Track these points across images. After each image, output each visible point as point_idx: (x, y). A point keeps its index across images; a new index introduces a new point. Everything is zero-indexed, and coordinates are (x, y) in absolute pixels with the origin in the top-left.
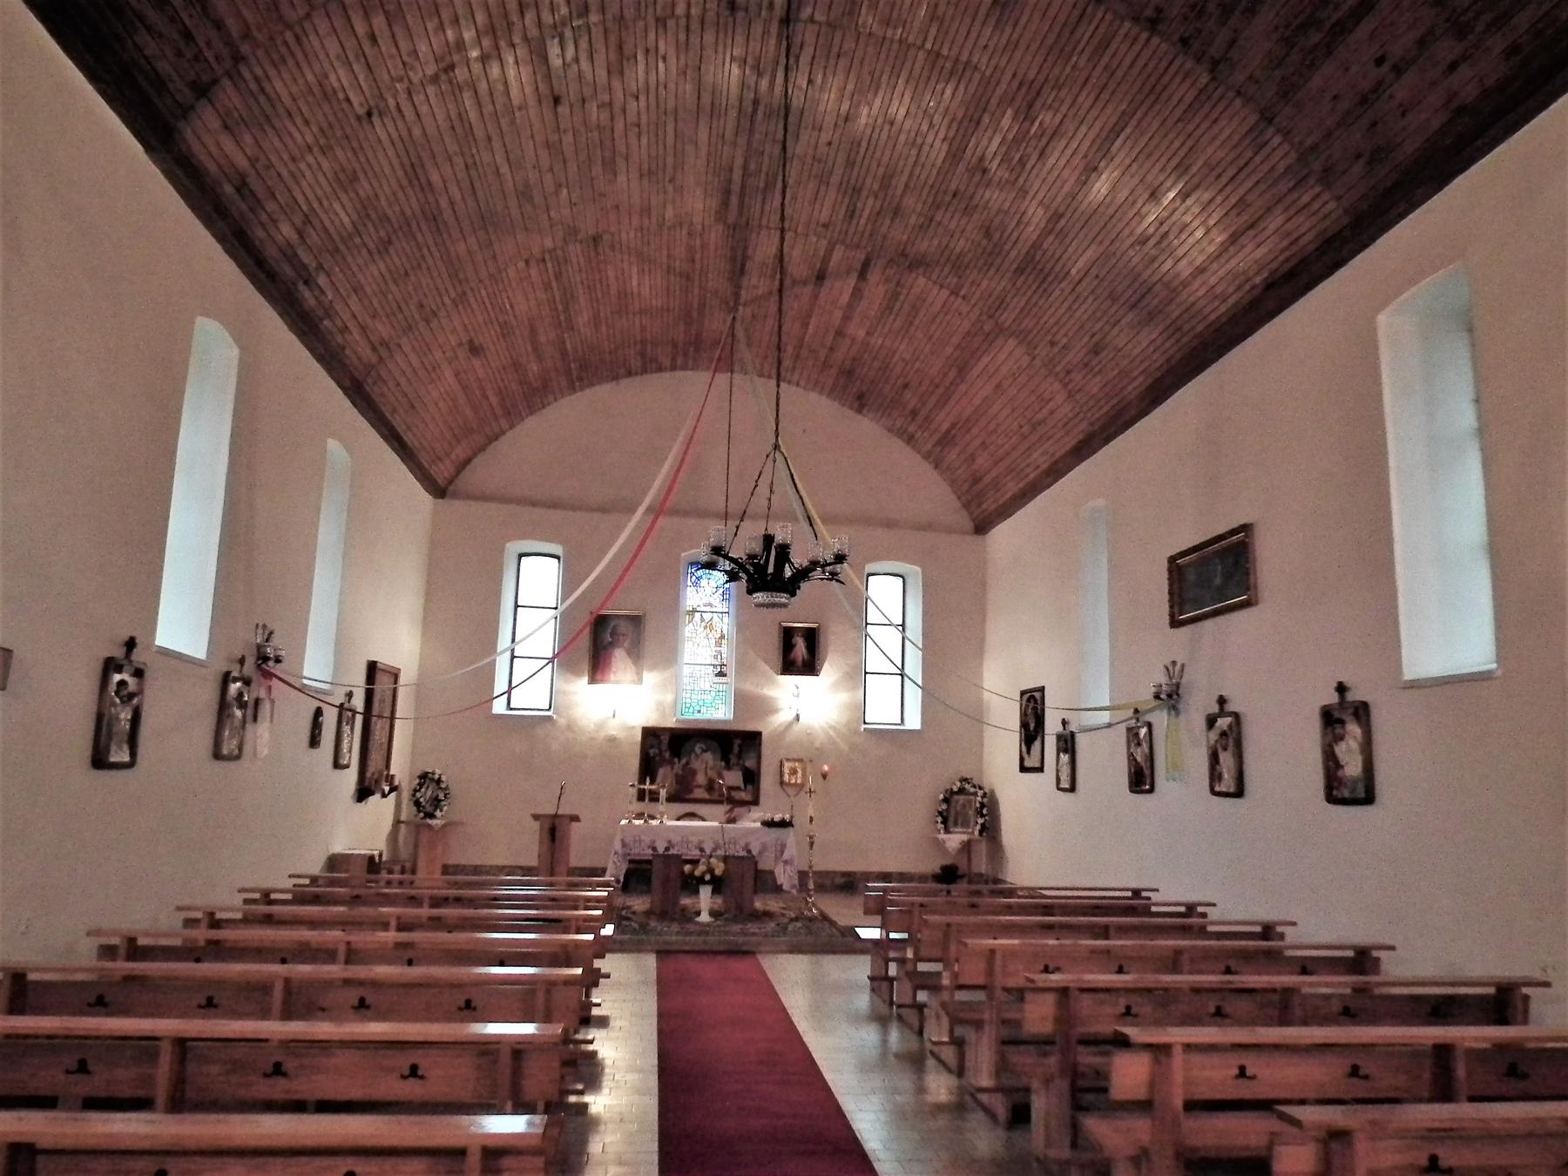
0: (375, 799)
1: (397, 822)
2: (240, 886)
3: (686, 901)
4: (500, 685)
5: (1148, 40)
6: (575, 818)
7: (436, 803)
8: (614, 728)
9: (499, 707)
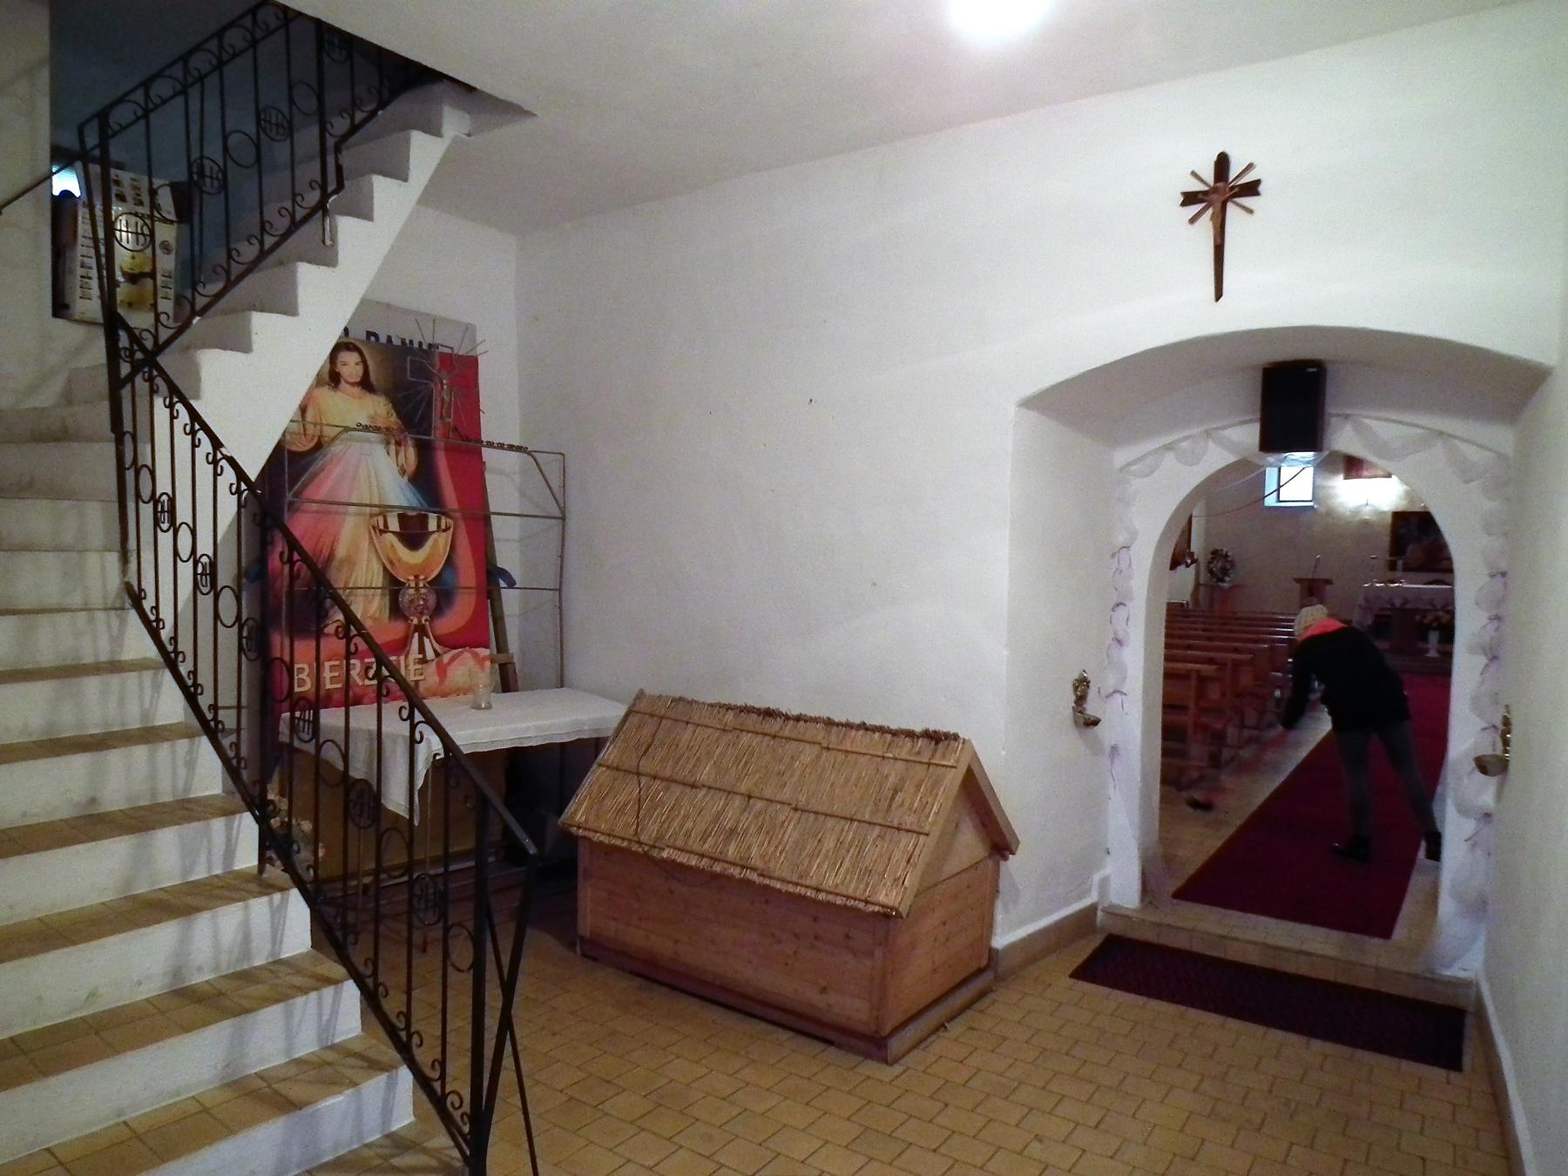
0: (1182, 568)
1: (1197, 585)
2: (1070, 740)
3: (1421, 645)
4: (1270, 486)
5: (331, 1069)
6: (1328, 582)
7: (1225, 571)
8: (1366, 514)
9: (1270, 501)
